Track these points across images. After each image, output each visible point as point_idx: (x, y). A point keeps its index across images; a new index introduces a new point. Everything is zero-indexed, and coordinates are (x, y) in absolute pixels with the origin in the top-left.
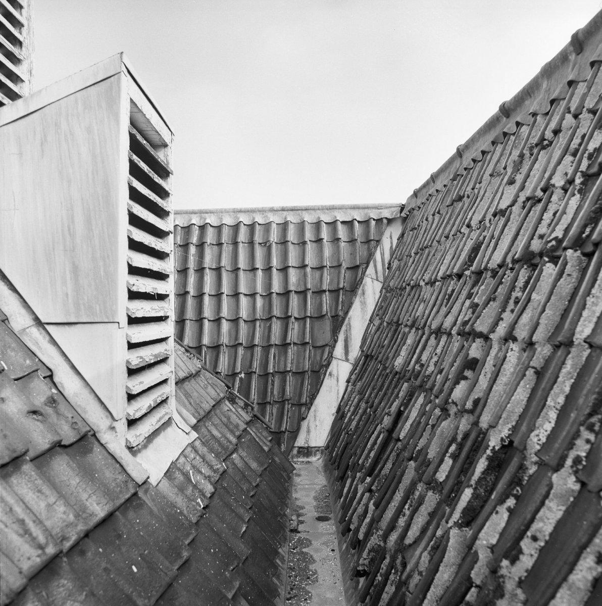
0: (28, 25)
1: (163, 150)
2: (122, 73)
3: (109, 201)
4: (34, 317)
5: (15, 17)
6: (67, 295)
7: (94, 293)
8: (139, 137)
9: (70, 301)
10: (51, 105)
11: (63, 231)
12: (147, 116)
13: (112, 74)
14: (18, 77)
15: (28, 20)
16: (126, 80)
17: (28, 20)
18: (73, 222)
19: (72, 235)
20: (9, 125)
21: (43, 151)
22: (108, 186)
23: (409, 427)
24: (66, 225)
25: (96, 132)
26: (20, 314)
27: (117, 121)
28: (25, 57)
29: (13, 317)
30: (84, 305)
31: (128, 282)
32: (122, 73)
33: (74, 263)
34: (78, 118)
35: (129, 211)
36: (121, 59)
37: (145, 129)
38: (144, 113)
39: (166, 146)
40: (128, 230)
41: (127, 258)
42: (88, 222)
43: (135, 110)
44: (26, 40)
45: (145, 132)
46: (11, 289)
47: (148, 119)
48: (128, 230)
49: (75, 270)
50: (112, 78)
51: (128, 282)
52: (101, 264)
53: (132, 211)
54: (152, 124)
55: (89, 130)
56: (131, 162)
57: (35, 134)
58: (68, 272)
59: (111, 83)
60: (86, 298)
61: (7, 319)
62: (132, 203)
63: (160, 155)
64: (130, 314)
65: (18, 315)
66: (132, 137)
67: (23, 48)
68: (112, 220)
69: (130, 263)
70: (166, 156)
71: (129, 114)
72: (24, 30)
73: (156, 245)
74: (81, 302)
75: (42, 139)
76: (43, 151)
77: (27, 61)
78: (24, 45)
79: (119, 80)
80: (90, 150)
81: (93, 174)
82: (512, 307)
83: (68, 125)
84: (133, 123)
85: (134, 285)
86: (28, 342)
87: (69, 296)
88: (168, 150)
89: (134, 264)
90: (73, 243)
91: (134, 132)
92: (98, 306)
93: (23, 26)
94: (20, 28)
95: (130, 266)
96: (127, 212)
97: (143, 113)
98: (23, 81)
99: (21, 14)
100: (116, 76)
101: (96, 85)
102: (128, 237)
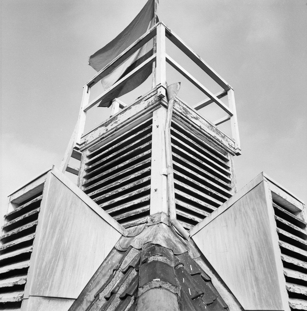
0: (233, 174)
1: (300, 213)
2: (264, 181)
3: (267, 242)
4: (240, 307)
5: (226, 172)
6: (254, 294)
7: (268, 293)
8: (279, 208)
9: (256, 298)
10: (236, 202)
11: (248, 259)
12: (283, 198)
13: (260, 182)
14: (231, 195)
15: (232, 171)
16: (266, 184)
17: (232, 171)
18: (252, 254)
19: (253, 261)
20: (221, 214)
21: (235, 223)
22: (266, 235)
23: (129, 305)
24: (249, 256)
25: (257, 209)
26: (234, 305)
27: (265, 202)
28: (233, 186)
29: (230, 306)
30: (264, 300)
31: (286, 287)
32: (264, 181)
33: (255, 276)
34: (248, 205)
35: (280, 246)
36: (263, 175)
37: (285, 204)
38: (281, 196)
39: (300, 211)
40: (281, 257)
41: (283, 272)
42: (259, 254)
43: (274, 194)
44: (232, 180)
45: (286, 206)
46: (229, 292)
47: (285, 199)
48: (281, 257)
49: (257, 279)
50: (260, 184)
51: (286, 287)
52: (269, 276)
53: (281, 246)
54: (288, 201)
55: (254, 209)
56: (277, 221)
57: (232, 216)
58: (253, 281)
59: (260, 187)
60: (264, 296)
61: (228, 307)
62: (281, 242)
63: (298, 217)
64: (291, 306)
65: (233, 306)
66: (275, 209)
67: (232, 183)
68: (271, 252)
69: (286, 275)
70: (302, 216)
71: (272, 198)
72: (231, 177)
73: (303, 265)
74: (262, 298)
75: (234, 218)
76: (235, 223)
77: (233, 188)
78: (232, 181)
79: (263, 184)
80: (255, 218)
81: (258, 229)
82: (93, 193)
83: (244, 209)
84: (274, 201)
85: (290, 288)
86: (176, 304)
87: (256, 294)
88: (303, 213)
89: (288, 276)
90: (254, 265)
91: (276, 205)
92: (271, 300)
93: (230, 174)
94: (230, 176)
95: (286, 277)
96: (279, 247)
97: (280, 196)
98: (232, 196)
99: (229, 170)
100: (262, 183)
101: (253, 189)
102: (282, 260)
